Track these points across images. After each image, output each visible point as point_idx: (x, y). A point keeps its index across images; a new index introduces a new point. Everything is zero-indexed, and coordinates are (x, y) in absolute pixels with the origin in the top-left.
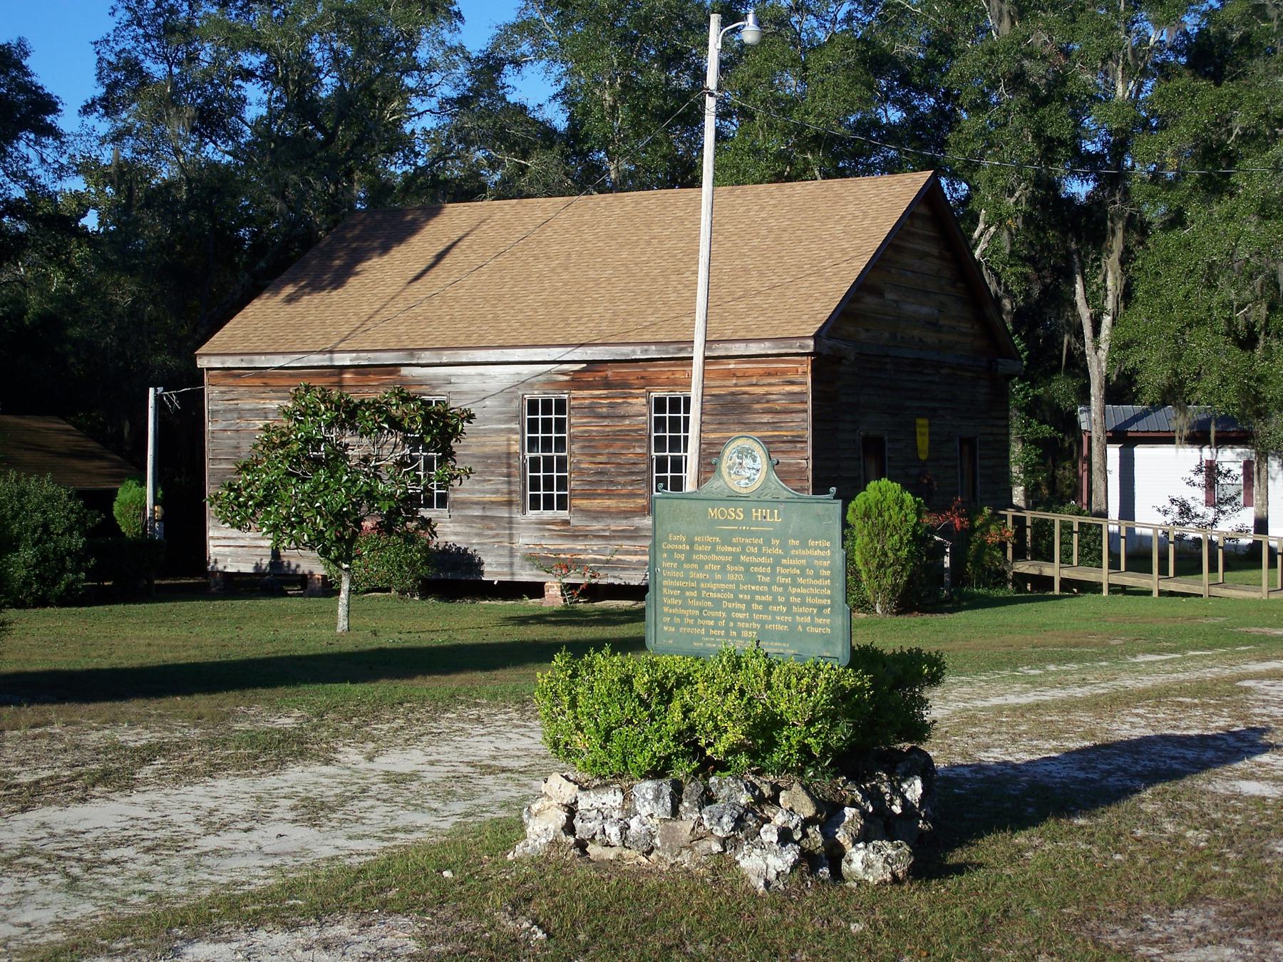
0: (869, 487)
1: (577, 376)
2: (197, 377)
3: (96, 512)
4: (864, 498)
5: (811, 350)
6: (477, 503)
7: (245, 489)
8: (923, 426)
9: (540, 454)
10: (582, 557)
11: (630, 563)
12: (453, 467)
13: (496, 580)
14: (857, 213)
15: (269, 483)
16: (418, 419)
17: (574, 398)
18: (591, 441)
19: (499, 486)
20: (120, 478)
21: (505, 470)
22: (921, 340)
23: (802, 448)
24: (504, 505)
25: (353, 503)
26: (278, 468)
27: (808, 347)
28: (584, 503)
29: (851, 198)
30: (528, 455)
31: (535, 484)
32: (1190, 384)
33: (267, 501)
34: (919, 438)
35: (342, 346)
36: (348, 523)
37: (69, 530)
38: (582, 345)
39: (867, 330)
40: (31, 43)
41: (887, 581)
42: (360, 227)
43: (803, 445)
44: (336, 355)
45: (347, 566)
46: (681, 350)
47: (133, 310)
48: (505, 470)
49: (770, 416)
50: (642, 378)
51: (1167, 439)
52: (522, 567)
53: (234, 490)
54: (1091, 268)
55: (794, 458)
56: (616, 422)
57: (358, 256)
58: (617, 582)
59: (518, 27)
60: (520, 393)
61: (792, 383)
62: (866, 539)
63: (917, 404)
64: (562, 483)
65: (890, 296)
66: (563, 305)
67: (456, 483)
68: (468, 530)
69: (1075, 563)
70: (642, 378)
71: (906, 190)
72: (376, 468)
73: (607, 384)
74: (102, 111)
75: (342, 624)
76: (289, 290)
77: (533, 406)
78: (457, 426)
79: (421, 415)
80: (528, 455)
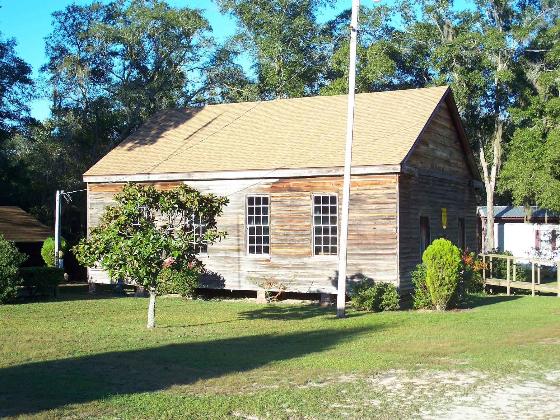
0: (434, 242)
1: (275, 185)
2: (85, 185)
3: (25, 254)
4: (432, 249)
5: (399, 171)
6: (222, 250)
7: (94, 243)
8: (444, 212)
9: (321, 225)
10: (276, 278)
11: (301, 281)
12: (216, 231)
13: (232, 289)
14: (413, 105)
15: (108, 240)
16: (196, 202)
17: (272, 197)
18: (281, 218)
19: (234, 242)
20: (46, 236)
21: (236, 234)
22: (443, 169)
23: (394, 222)
24: (235, 251)
25: (157, 252)
26: (113, 231)
27: (398, 169)
28: (278, 251)
29: (409, 99)
30: (249, 226)
31: (252, 240)
32: (537, 196)
33: (107, 250)
34: (443, 218)
35: (155, 171)
36: (153, 264)
37: (10, 264)
38: (277, 169)
39: (422, 163)
40: (18, 40)
41: (444, 293)
42: (164, 116)
43: (394, 221)
44: (150, 176)
45: (153, 289)
46: (329, 171)
47: (60, 159)
48: (236, 234)
49: (377, 205)
50: (308, 186)
51: (520, 221)
52: (245, 283)
53: (88, 244)
54: (487, 145)
55: (389, 228)
56: (295, 209)
57: (163, 129)
58: (294, 291)
59: (236, 37)
60: (245, 194)
61: (388, 188)
62: (433, 271)
63: (441, 201)
64: (266, 240)
65: (431, 146)
66: (266, 150)
67: (217, 240)
68: (218, 264)
69: (514, 280)
70: (308, 186)
71: (437, 94)
72: (171, 231)
73: (290, 190)
74: (50, 71)
75: (150, 323)
76: (130, 145)
77: (251, 201)
78: (218, 207)
79: (198, 200)
80: (249, 226)
